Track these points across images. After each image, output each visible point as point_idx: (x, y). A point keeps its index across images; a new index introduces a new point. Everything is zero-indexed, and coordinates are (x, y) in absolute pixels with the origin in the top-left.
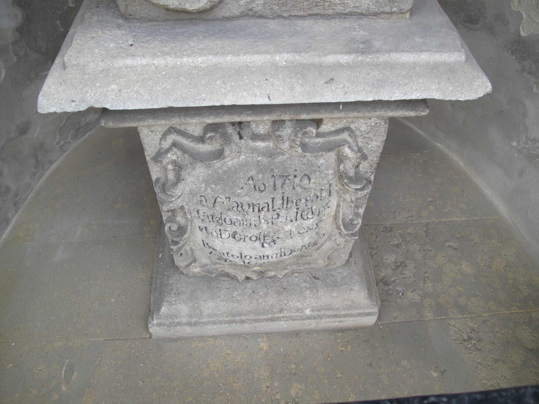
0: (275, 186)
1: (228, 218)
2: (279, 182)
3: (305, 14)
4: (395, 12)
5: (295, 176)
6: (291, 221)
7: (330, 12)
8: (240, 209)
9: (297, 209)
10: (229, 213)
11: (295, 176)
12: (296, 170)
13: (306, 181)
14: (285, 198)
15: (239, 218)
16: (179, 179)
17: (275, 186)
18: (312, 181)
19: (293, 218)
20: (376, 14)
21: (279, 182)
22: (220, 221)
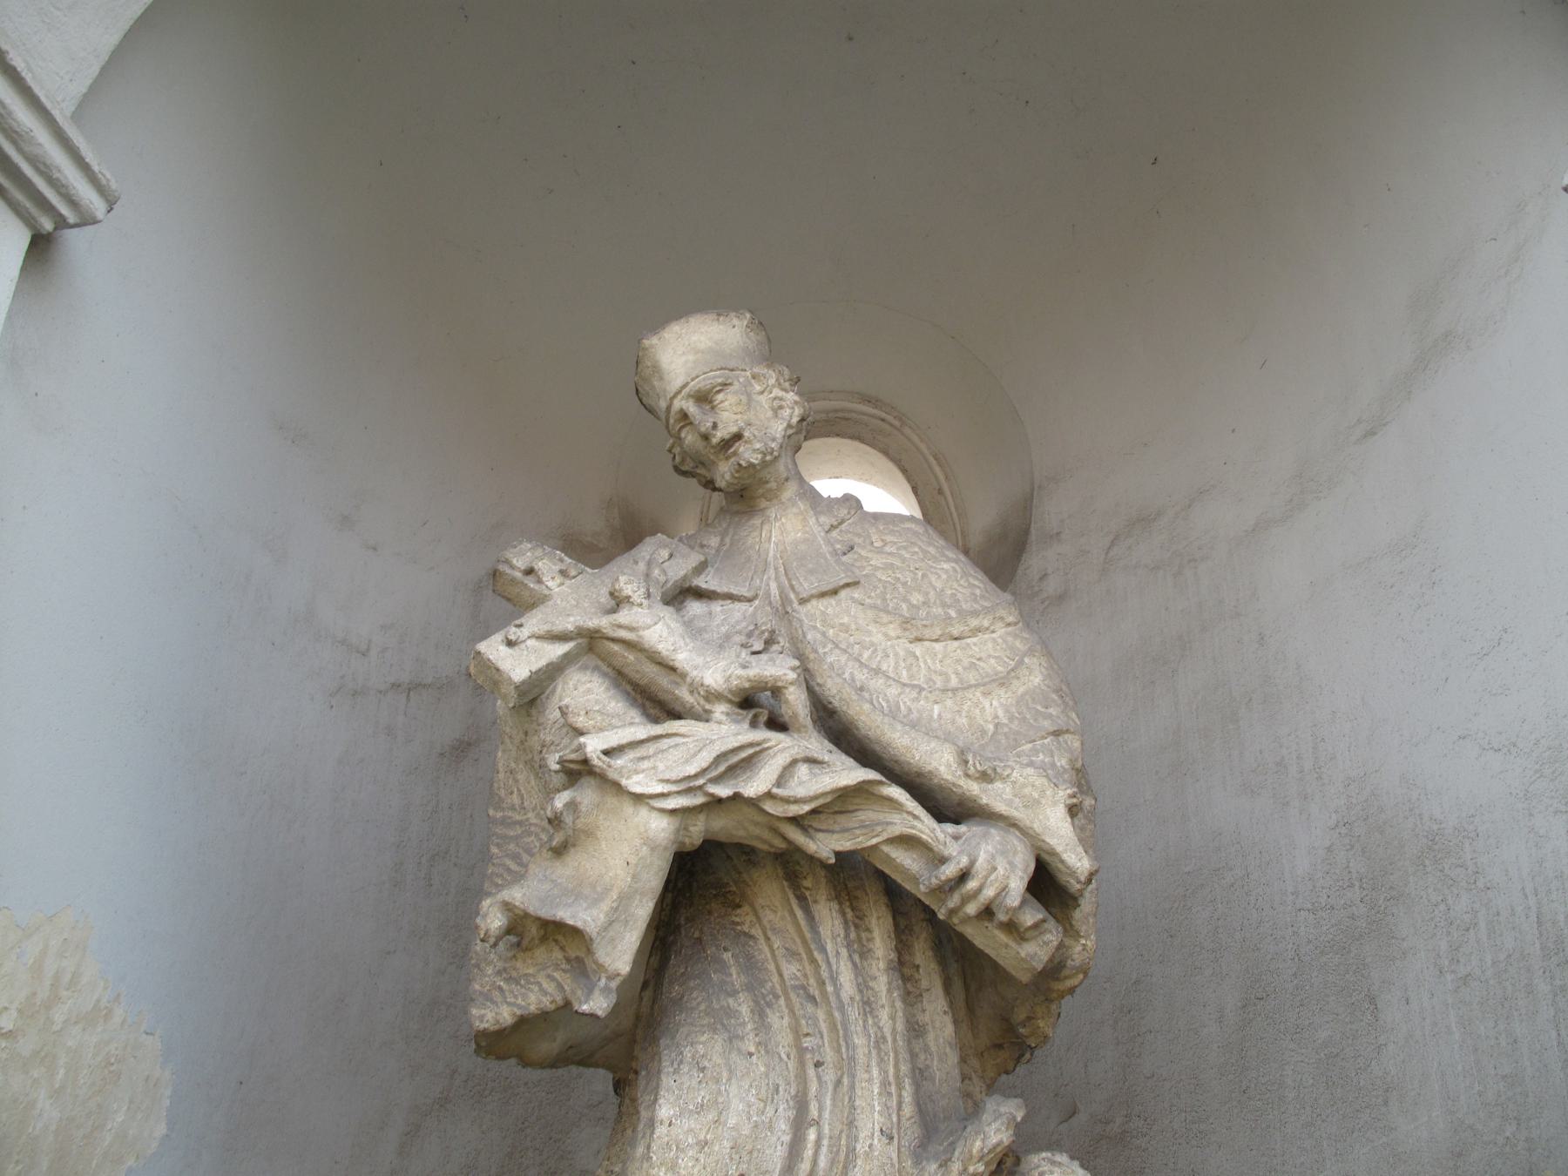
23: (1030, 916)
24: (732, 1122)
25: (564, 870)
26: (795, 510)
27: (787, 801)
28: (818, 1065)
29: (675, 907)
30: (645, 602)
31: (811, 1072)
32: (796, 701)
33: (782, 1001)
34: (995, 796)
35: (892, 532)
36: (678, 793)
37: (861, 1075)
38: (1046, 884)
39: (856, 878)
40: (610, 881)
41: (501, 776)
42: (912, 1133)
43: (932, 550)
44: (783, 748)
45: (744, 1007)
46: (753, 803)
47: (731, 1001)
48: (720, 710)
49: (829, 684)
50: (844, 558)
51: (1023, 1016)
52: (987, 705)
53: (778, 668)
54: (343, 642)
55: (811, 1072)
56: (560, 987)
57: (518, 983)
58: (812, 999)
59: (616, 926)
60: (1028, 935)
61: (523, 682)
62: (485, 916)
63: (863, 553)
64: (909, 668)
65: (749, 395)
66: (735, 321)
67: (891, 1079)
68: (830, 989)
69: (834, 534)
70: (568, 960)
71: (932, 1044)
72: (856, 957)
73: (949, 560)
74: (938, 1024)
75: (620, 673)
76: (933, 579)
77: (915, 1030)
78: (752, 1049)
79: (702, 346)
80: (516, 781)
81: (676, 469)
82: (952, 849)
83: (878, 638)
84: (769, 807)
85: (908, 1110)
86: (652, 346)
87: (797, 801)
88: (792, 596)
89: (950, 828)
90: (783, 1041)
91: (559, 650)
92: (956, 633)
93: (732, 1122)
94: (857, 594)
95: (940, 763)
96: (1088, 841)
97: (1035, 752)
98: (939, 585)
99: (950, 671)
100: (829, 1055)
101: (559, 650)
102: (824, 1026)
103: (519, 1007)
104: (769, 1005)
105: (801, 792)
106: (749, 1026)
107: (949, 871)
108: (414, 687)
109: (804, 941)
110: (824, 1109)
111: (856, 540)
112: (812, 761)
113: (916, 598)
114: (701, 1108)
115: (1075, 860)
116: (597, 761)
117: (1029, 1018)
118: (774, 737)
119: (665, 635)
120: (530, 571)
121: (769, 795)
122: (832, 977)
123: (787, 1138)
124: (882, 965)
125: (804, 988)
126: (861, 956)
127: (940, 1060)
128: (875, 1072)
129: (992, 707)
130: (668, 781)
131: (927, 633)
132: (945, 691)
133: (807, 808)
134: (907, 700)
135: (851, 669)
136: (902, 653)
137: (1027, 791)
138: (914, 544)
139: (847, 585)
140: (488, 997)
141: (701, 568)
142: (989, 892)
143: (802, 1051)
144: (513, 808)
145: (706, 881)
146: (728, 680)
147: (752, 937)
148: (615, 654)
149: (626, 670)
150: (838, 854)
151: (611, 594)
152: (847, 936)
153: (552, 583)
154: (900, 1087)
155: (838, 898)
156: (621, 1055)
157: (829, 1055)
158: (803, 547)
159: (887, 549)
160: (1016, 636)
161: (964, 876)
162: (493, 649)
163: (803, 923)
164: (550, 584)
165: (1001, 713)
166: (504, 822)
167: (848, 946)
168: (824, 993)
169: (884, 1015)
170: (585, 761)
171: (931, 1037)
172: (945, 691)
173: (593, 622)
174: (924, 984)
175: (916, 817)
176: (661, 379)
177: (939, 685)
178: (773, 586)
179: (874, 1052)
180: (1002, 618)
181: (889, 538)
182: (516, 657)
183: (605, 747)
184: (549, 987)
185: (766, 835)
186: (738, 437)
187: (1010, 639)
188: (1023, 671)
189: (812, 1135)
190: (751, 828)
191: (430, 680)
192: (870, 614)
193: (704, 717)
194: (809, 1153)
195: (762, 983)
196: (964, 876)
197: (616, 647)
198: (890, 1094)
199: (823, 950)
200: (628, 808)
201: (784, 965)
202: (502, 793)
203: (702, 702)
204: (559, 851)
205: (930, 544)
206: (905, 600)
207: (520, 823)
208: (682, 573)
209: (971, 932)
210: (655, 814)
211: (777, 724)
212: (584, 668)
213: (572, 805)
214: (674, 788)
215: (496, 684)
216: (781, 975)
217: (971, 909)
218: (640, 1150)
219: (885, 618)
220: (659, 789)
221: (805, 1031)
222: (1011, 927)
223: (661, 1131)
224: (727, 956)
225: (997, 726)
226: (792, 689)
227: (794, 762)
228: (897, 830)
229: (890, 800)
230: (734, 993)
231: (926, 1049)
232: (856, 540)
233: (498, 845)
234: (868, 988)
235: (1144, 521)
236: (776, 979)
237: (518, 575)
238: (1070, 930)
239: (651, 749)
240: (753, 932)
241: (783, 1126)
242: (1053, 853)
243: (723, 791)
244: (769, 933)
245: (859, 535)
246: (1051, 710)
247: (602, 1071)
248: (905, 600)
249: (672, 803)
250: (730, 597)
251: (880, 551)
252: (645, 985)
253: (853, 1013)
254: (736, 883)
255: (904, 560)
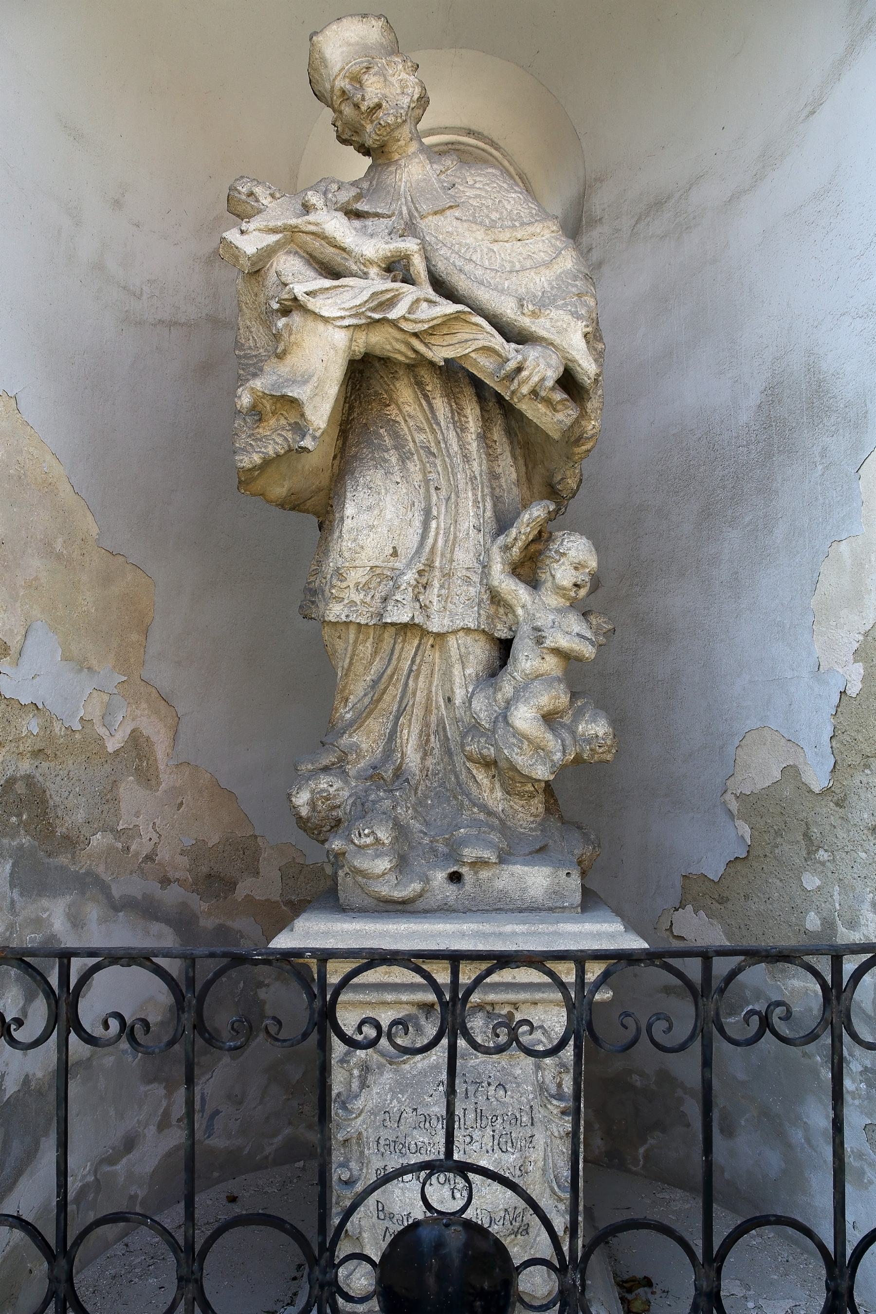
0: (467, 1094)
1: (413, 1143)
2: (472, 1089)
3: (491, 909)
4: (566, 907)
5: (489, 1084)
6: (487, 1152)
7: (511, 907)
8: (427, 1124)
9: (494, 1131)
10: (415, 1132)
11: (489, 1084)
12: (490, 1077)
13: (502, 1092)
14: (479, 1111)
15: (426, 1141)
16: (363, 1085)
17: (467, 1094)
18: (509, 1093)
19: (489, 1148)
20: (551, 909)
21: (472, 1089)
22: (403, 1151)
23: (559, 396)
24: (389, 517)
25: (284, 369)
26: (417, 160)
27: (415, 321)
28: (437, 489)
29: (351, 409)
30: (325, 208)
31: (433, 491)
32: (419, 266)
33: (415, 457)
34: (538, 327)
35: (480, 175)
36: (350, 316)
37: (462, 495)
38: (569, 382)
39: (455, 376)
40: (316, 363)
41: (241, 331)
42: (491, 526)
43: (505, 185)
44: (410, 293)
45: (393, 458)
46: (394, 323)
47: (385, 454)
48: (373, 271)
49: (440, 264)
50: (449, 192)
51: (559, 478)
52: (538, 282)
53: (410, 245)
54: (124, 288)
55: (433, 491)
56: (286, 439)
57: (261, 441)
58: (434, 455)
59: (317, 399)
60: (559, 407)
61: (253, 255)
62: (240, 397)
63: (461, 188)
64: (490, 259)
65: (384, 76)
66: (374, 22)
67: (479, 499)
68: (443, 446)
69: (443, 177)
70: (290, 425)
71: (504, 484)
72: (459, 430)
73: (516, 192)
74: (507, 472)
75: (311, 255)
76: (506, 203)
77: (494, 476)
78: (399, 480)
79: (352, 41)
80: (251, 332)
81: (339, 138)
82: (513, 354)
83: (470, 240)
84: (404, 325)
85: (489, 514)
86: (318, 42)
87: (422, 321)
88: (416, 214)
89: (513, 345)
90: (417, 478)
91: (273, 238)
92: (519, 237)
93: (389, 517)
94: (457, 213)
95: (508, 309)
96: (599, 357)
97: (566, 305)
98: (509, 207)
99: (515, 260)
100: (443, 483)
101: (273, 238)
102: (440, 469)
103: (263, 453)
104: (408, 458)
105: (423, 316)
106: (396, 468)
107: (512, 365)
108: (173, 324)
109: (427, 420)
110: (439, 510)
111: (457, 180)
112: (427, 300)
113: (495, 216)
114: (370, 508)
115: (587, 366)
116: (301, 297)
117: (563, 479)
118: (406, 287)
119: (337, 226)
120: (251, 194)
121: (404, 317)
122: (444, 440)
123: (420, 531)
124: (474, 437)
125: (427, 447)
126: (462, 430)
127: (509, 492)
128: (470, 494)
129: (539, 281)
130: (343, 309)
131: (501, 236)
132: (511, 272)
133: (426, 326)
134: (488, 276)
135: (454, 258)
136: (485, 250)
137: (559, 324)
138: (494, 182)
139: (451, 207)
140: (244, 449)
141: (358, 197)
142: (535, 379)
143: (427, 481)
144: (250, 348)
145: (364, 375)
146: (377, 251)
147: (397, 422)
148: (306, 243)
149: (314, 254)
150: (446, 360)
151: (303, 205)
152: (453, 418)
153: (265, 201)
154: (484, 500)
155: (447, 396)
156: (320, 509)
157: (443, 483)
158: (422, 184)
159: (477, 185)
160: (557, 239)
161: (519, 370)
162: (233, 236)
163: (426, 408)
164: (264, 202)
165: (546, 285)
166: (246, 356)
167: (454, 423)
168: (440, 450)
169: (475, 464)
170: (295, 299)
171: (503, 480)
172: (511, 272)
173: (293, 221)
174: (499, 451)
175: (492, 336)
176: (326, 67)
177: (508, 269)
178: (404, 209)
179: (470, 483)
180: (548, 228)
181: (478, 179)
182: (250, 241)
183: (305, 290)
184: (279, 440)
185: (403, 348)
186: (379, 106)
187: (553, 241)
188: (560, 259)
189: (434, 524)
190: (394, 343)
191: (183, 321)
192: (466, 225)
193: (365, 276)
194: (432, 534)
195: (403, 447)
196: (519, 370)
197: (308, 238)
198: (478, 507)
199: (438, 424)
200: (321, 326)
201: (416, 435)
202: (243, 341)
203: (362, 267)
204: (281, 356)
205: (504, 182)
206: (487, 216)
207: (255, 356)
208: (347, 199)
209: (524, 407)
210: (337, 329)
211: (408, 280)
212: (289, 252)
213: (286, 325)
214: (347, 313)
215: (237, 258)
216: (414, 441)
217: (525, 390)
218: (337, 534)
219: (475, 227)
220: (339, 314)
221: (429, 470)
222: (548, 401)
223: (348, 523)
224: (382, 431)
225: (543, 293)
226: (416, 256)
227: (417, 301)
228: (480, 344)
229: (476, 325)
230: (387, 451)
231: (500, 486)
232: (457, 180)
233: (243, 369)
234: (466, 448)
235: (658, 204)
236: (411, 444)
237: (244, 197)
238: (583, 414)
239: (333, 292)
240: (398, 419)
241: (417, 524)
242: (574, 361)
243: (377, 316)
244: (407, 418)
245: (459, 178)
246: (577, 283)
247: (310, 516)
248: (487, 216)
249: (346, 322)
250: (377, 215)
251: (472, 187)
252: (335, 458)
253: (458, 460)
254: (386, 392)
255: (487, 191)
